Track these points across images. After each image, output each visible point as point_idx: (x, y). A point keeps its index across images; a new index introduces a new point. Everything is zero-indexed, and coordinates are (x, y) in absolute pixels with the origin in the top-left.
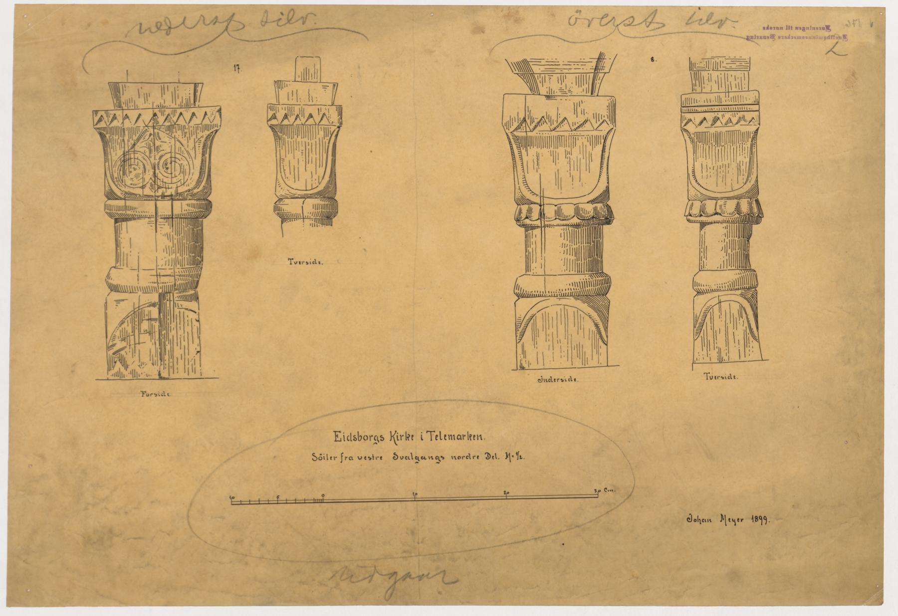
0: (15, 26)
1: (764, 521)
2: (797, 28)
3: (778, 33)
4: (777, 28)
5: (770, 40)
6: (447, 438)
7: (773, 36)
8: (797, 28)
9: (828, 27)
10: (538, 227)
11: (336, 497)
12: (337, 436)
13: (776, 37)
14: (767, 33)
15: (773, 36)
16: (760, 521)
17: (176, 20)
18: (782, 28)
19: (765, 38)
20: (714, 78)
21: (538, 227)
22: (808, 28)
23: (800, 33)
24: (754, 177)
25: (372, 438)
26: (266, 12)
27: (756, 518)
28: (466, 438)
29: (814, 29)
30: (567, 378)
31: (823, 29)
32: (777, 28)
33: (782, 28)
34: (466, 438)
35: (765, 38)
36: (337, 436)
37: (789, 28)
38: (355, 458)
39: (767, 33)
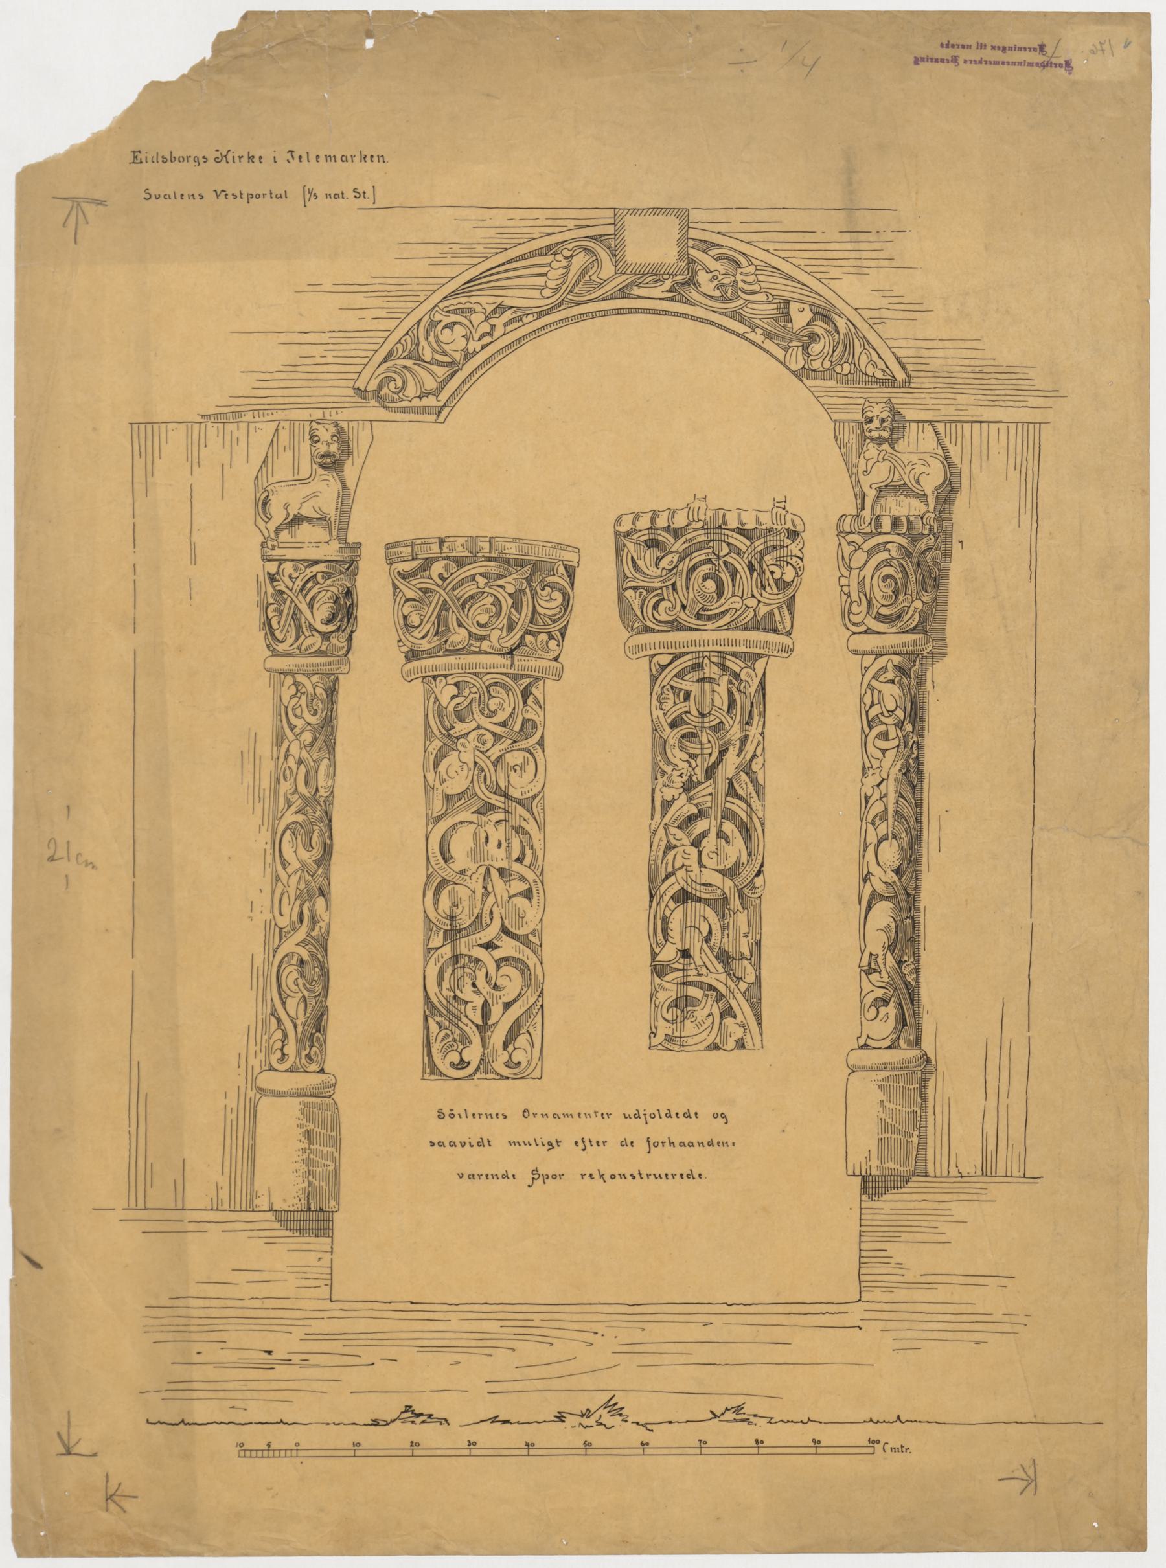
0: (15, 611)
2: (993, 48)
3: (963, 54)
5: (952, 65)
8: (993, 48)
9: (1042, 47)
12: (136, 157)
13: (961, 61)
14: (947, 53)
15: (955, 59)
17: (945, 515)
18: (969, 47)
19: (942, 61)
22: (1010, 48)
23: (998, 55)
25: (191, 160)
26: (413, 545)
28: (357, 159)
31: (1035, 49)
34: (357, 159)
36: (136, 157)
37: (981, 46)
38: (551, 1116)
39: (947, 53)
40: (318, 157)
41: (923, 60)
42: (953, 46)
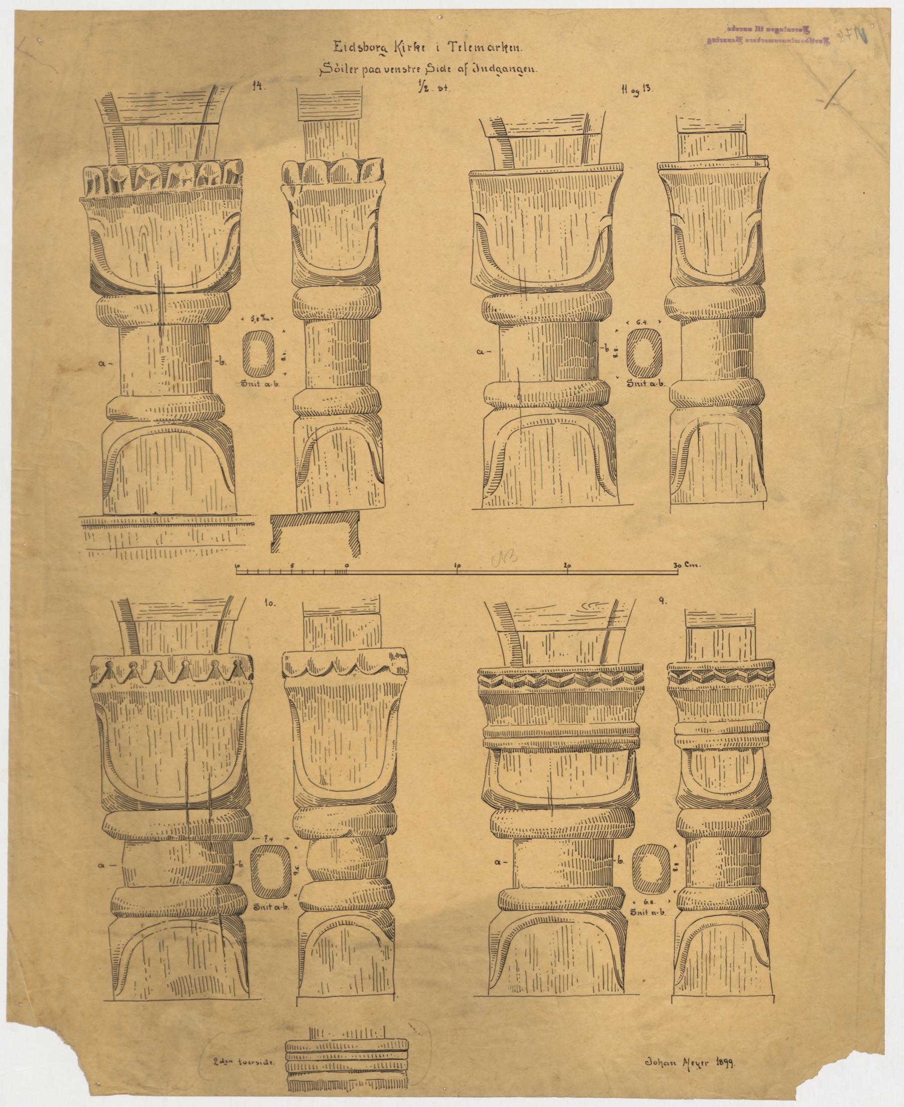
1: (730, 1065)
2: (768, 30)
3: (746, 35)
4: (745, 29)
6: (473, 49)
7: (739, 39)
8: (768, 30)
10: (155, 293)
11: (306, 567)
13: (744, 40)
15: (739, 39)
16: (725, 1064)
18: (750, 30)
19: (729, 40)
20: (592, 295)
21: (155, 293)
24: (233, 252)
27: (721, 1061)
29: (789, 30)
30: (263, 1061)
32: (745, 29)
33: (750, 30)
35: (729, 40)
39: (733, 35)
40: (351, 68)
41: (714, 40)
42: (737, 29)
